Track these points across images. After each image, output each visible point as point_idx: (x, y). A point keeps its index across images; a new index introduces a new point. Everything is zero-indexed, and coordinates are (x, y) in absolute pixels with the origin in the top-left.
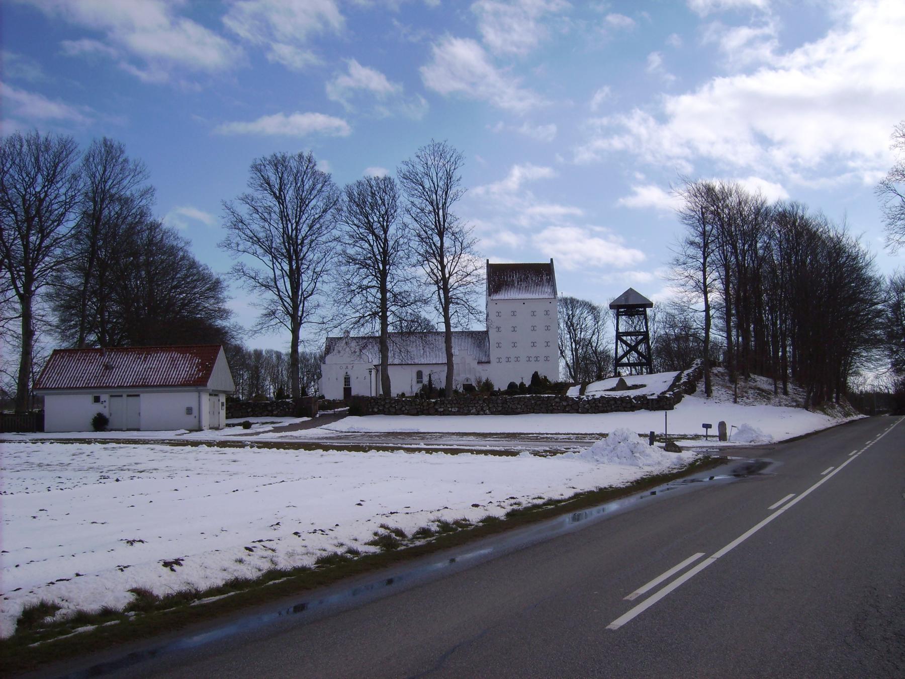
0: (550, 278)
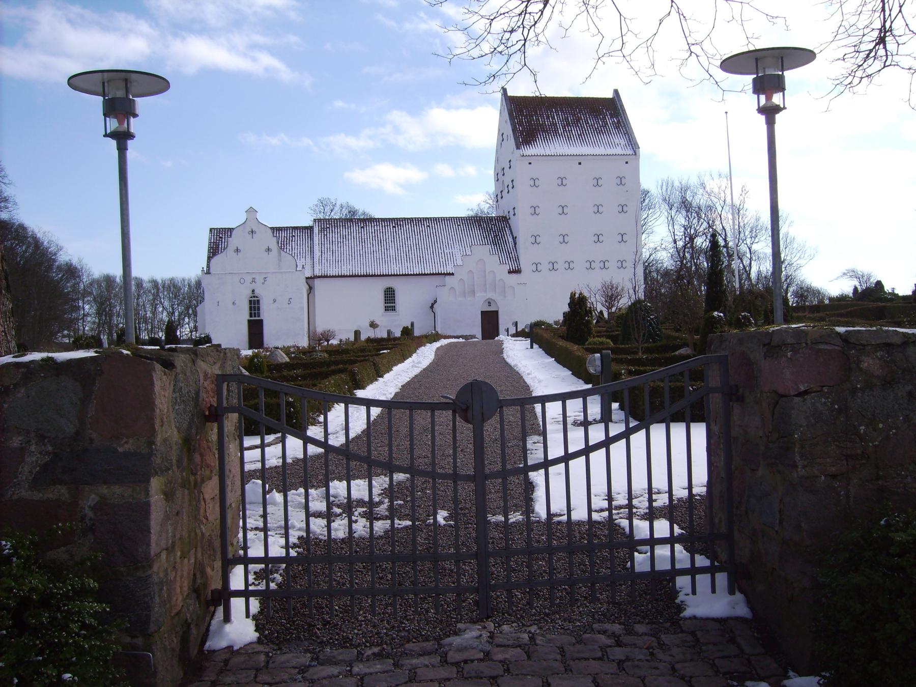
0: (619, 121)
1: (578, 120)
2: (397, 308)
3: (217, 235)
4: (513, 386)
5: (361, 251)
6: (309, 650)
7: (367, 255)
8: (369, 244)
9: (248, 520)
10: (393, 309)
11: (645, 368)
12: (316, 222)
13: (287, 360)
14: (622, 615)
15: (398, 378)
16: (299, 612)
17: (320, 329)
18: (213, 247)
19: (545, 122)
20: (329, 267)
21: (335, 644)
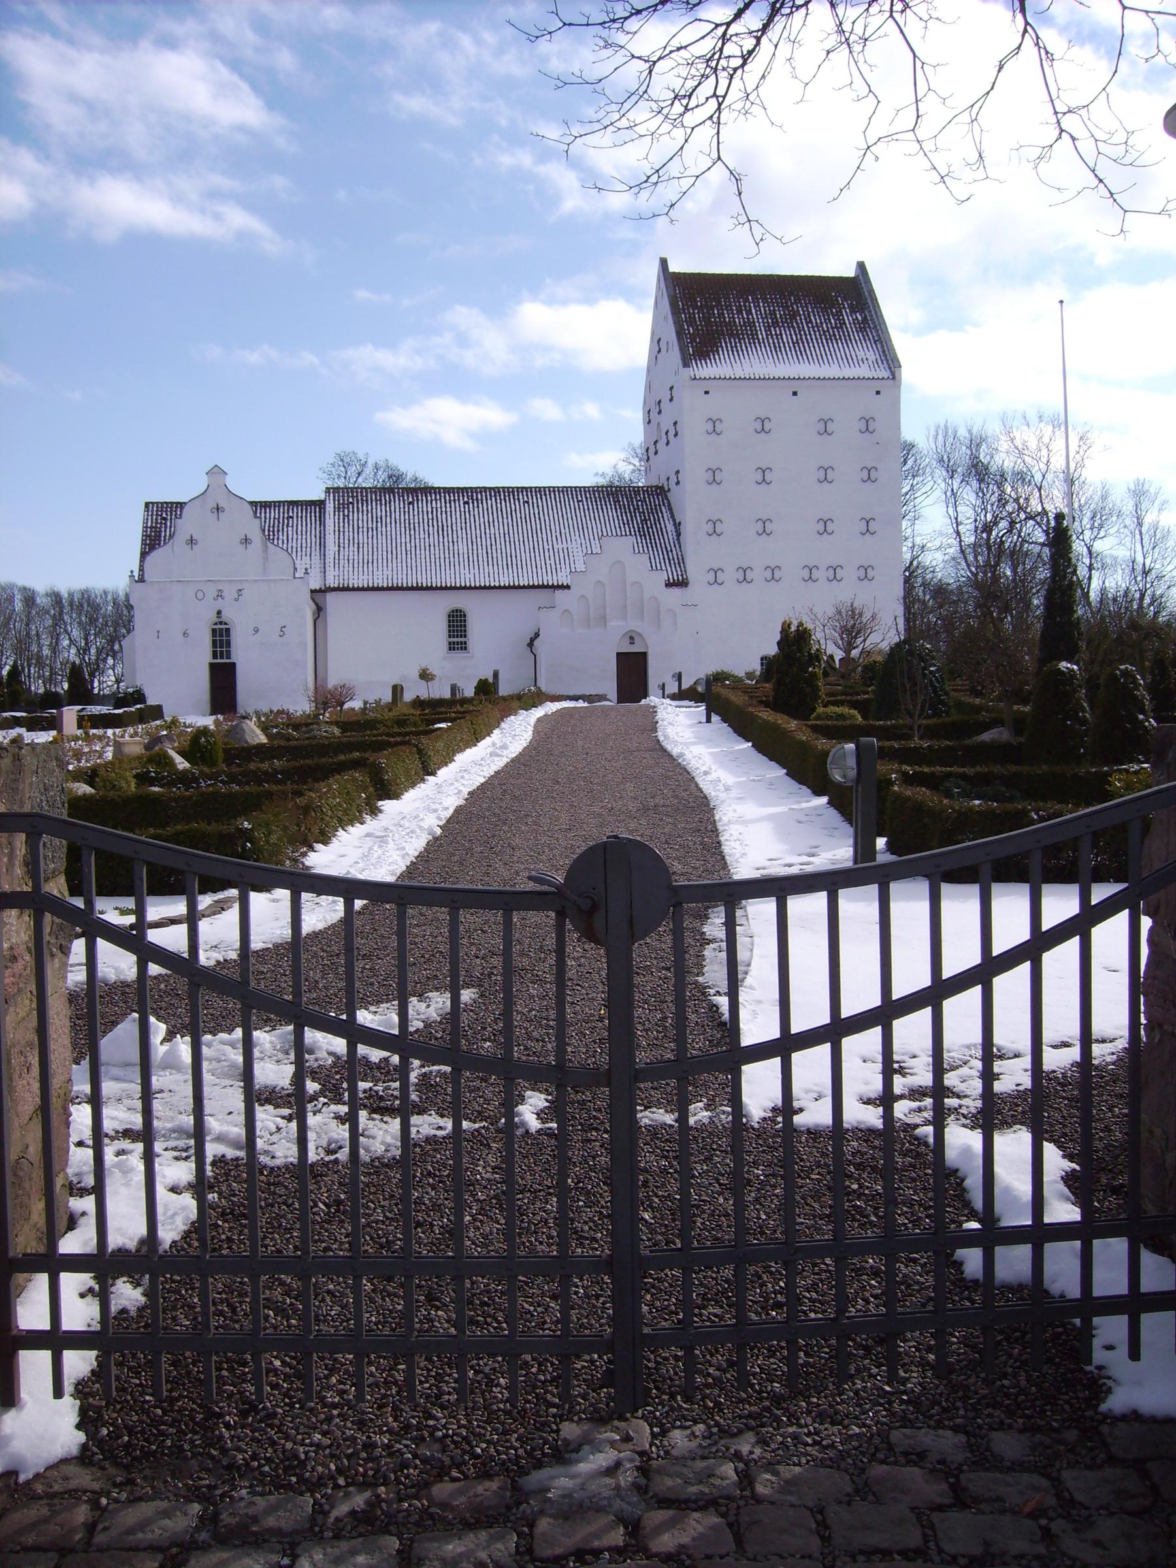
0: (865, 319)
1: (794, 316)
2: (470, 646)
3: (157, 515)
4: (676, 797)
5: (408, 545)
6: (198, 1488)
7: (418, 552)
8: (422, 532)
9: (106, 1112)
10: (463, 647)
11: (933, 769)
12: (329, 493)
13: (263, 739)
14: (959, 1404)
15: (463, 777)
16: (189, 1373)
17: (332, 681)
18: (150, 536)
19: (734, 318)
20: (351, 573)
21: (262, 1474)
